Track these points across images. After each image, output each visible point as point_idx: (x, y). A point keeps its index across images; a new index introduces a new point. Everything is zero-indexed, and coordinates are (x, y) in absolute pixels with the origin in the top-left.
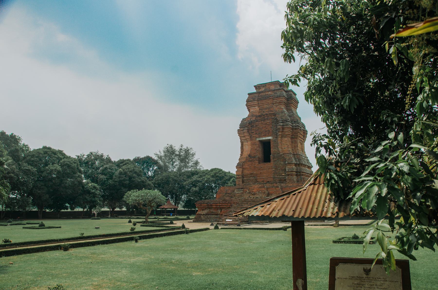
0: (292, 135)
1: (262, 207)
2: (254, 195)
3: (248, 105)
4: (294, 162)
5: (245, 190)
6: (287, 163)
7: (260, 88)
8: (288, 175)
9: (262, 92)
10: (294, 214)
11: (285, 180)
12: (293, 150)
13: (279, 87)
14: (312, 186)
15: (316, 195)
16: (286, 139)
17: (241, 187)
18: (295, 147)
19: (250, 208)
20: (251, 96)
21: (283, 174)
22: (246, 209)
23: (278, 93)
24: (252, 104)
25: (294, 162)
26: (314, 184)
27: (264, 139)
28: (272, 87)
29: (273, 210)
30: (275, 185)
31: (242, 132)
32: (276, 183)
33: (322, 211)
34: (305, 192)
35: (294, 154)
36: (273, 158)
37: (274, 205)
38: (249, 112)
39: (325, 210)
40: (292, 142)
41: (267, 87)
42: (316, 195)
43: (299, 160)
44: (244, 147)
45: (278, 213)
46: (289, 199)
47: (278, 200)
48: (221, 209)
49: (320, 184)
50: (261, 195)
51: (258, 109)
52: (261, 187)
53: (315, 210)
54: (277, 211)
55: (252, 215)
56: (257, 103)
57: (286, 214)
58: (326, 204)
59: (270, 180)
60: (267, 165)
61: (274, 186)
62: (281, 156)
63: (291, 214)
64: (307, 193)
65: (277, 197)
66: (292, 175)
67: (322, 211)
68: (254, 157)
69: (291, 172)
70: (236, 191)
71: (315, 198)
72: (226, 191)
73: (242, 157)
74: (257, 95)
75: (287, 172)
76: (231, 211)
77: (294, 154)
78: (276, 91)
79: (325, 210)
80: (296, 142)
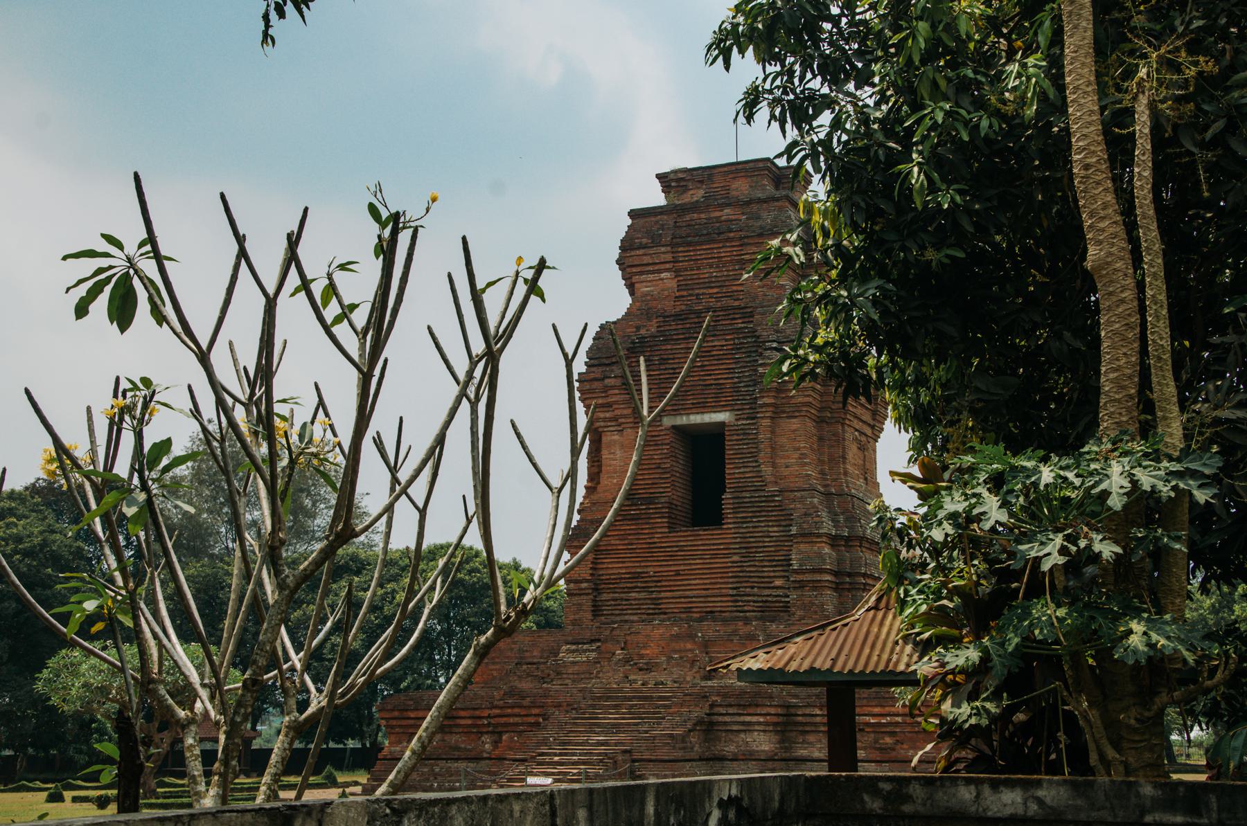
0: (820, 410)
1: (767, 653)
2: (648, 670)
3: (629, 262)
4: (827, 527)
5: (609, 646)
6: (794, 530)
7: (685, 189)
8: (801, 585)
9: (694, 207)
10: (833, 666)
11: (786, 608)
12: (822, 473)
13: (770, 189)
14: (872, 612)
15: (879, 630)
16: (795, 424)
17: (588, 635)
18: (832, 459)
19: (742, 655)
20: (641, 221)
21: (778, 583)
22: (733, 658)
23: (764, 215)
24: (646, 260)
25: (827, 527)
26: (876, 608)
27: (696, 419)
28: (741, 188)
29: (791, 659)
30: (744, 629)
31: (596, 385)
32: (747, 621)
33: (889, 660)
34: (857, 624)
35: (828, 495)
36: (736, 510)
37: (793, 650)
38: (632, 293)
39: (894, 660)
40: (821, 439)
41: (718, 183)
42: (879, 630)
43: (852, 519)
44: (605, 454)
45: (801, 665)
46: (823, 638)
47: (798, 639)
48: (497, 733)
49: (888, 608)
50: (677, 672)
51: (674, 284)
52: (677, 637)
53: (875, 658)
54: (798, 660)
55: (749, 669)
56: (669, 257)
57: (817, 665)
58: (898, 648)
59: (718, 604)
60: (708, 538)
61: (735, 632)
62: (770, 498)
63: (827, 665)
64: (861, 625)
65: (798, 635)
66: (816, 586)
67: (889, 660)
68: (650, 501)
69: (814, 571)
70: (566, 655)
71: (877, 637)
72: (521, 651)
73: (595, 497)
74: (668, 220)
75: (795, 572)
76: (544, 742)
77: (828, 495)
78: (755, 207)
79: (894, 660)
80: (839, 440)
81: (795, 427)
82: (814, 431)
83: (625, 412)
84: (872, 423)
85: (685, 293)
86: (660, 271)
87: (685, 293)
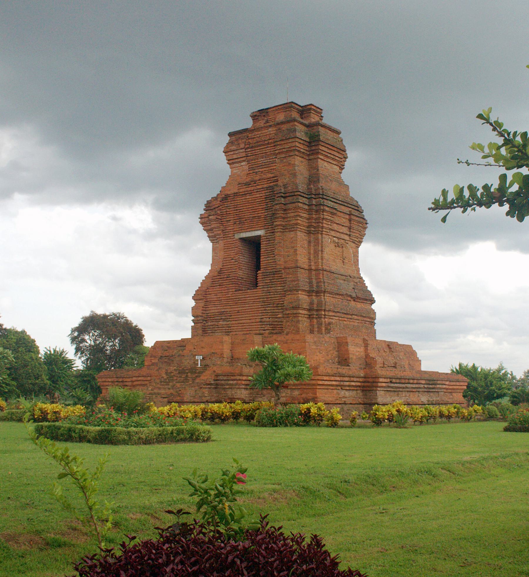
0: (308, 227)
60: (252, 293)
81: (292, 236)
82: (306, 238)
83: (219, 232)
84: (348, 233)
85: (251, 172)
86: (240, 162)
87: (251, 172)
